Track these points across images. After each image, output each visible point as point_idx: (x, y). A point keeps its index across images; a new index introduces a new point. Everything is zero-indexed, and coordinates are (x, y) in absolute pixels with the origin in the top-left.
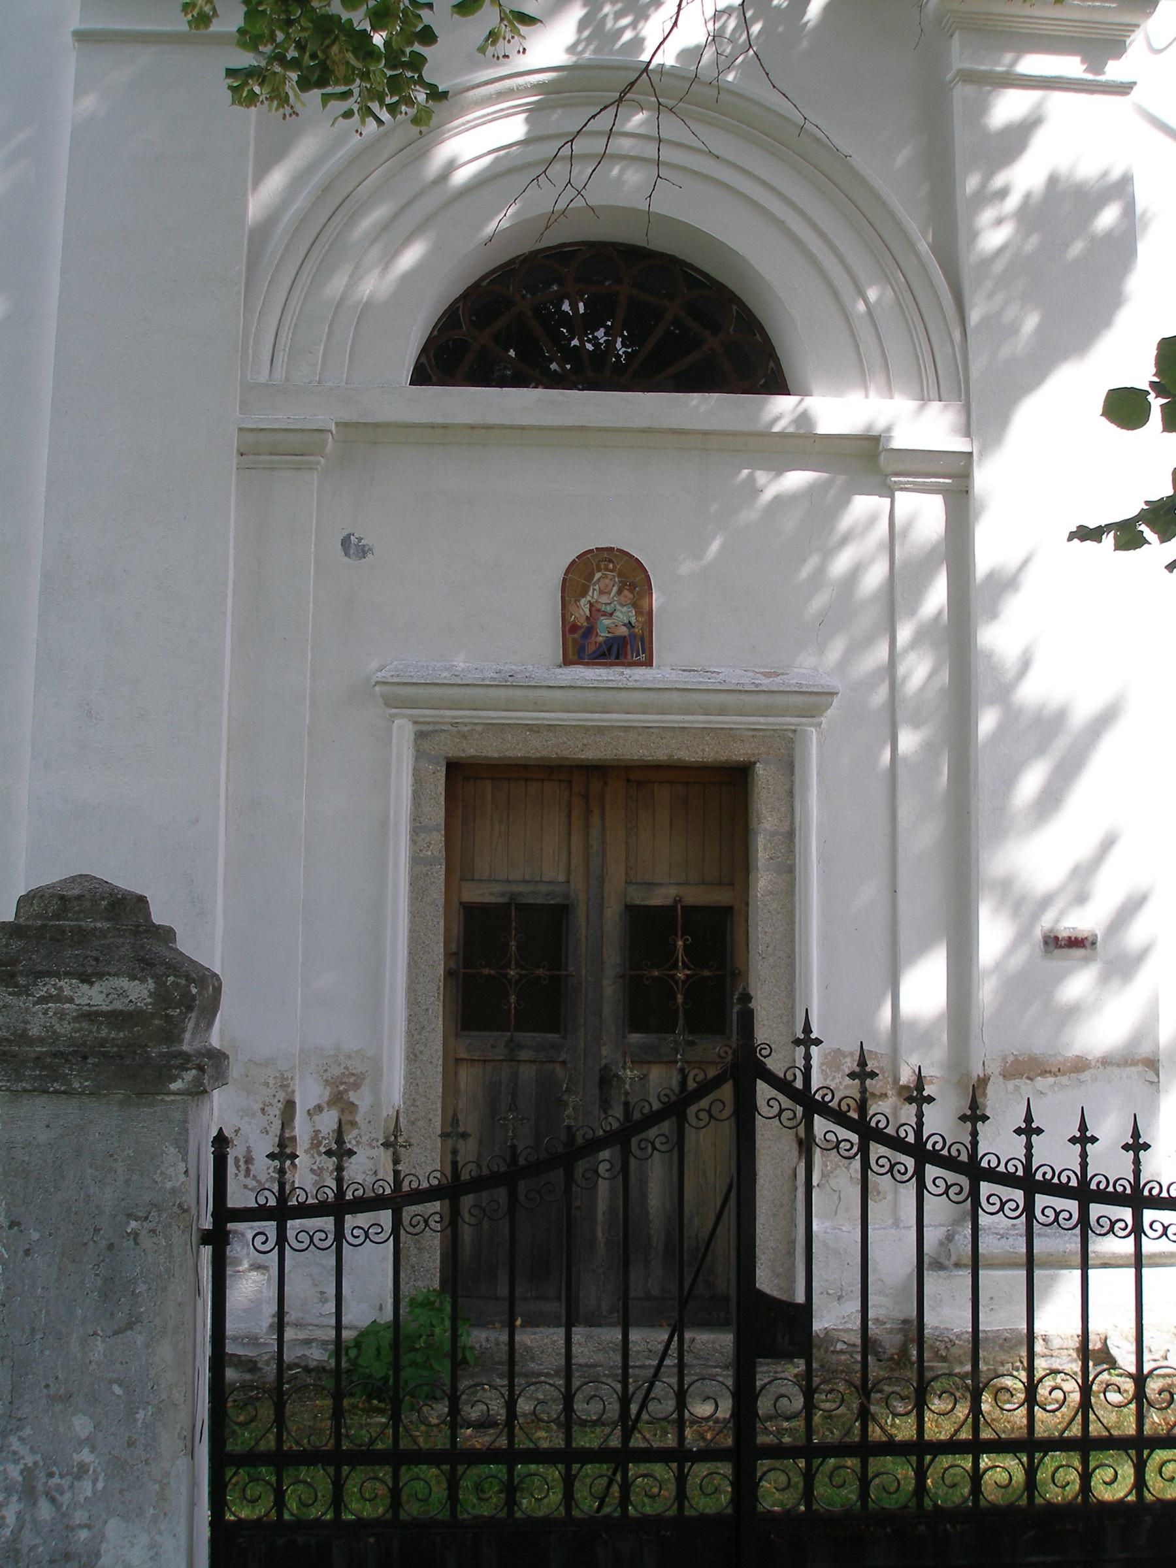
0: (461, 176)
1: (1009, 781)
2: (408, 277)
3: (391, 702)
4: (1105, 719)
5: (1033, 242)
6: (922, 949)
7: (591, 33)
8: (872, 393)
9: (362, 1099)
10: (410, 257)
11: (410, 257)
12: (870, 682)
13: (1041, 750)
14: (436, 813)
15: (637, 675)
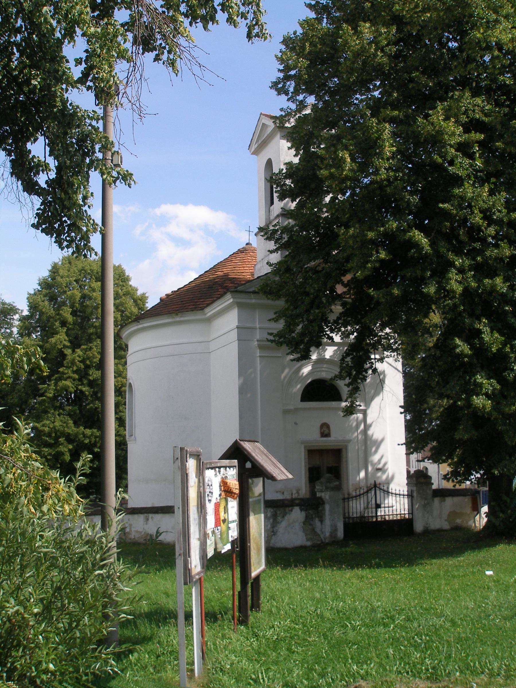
0: (304, 375)
1: (371, 450)
2: (299, 388)
3: (302, 443)
4: (382, 440)
5: (372, 381)
6: (362, 470)
7: (16, 48)
8: (147, 301)
9: (300, 492)
10: (299, 386)
11: (299, 386)
12: (355, 437)
13: (375, 445)
14: (307, 456)
15: (329, 439)
